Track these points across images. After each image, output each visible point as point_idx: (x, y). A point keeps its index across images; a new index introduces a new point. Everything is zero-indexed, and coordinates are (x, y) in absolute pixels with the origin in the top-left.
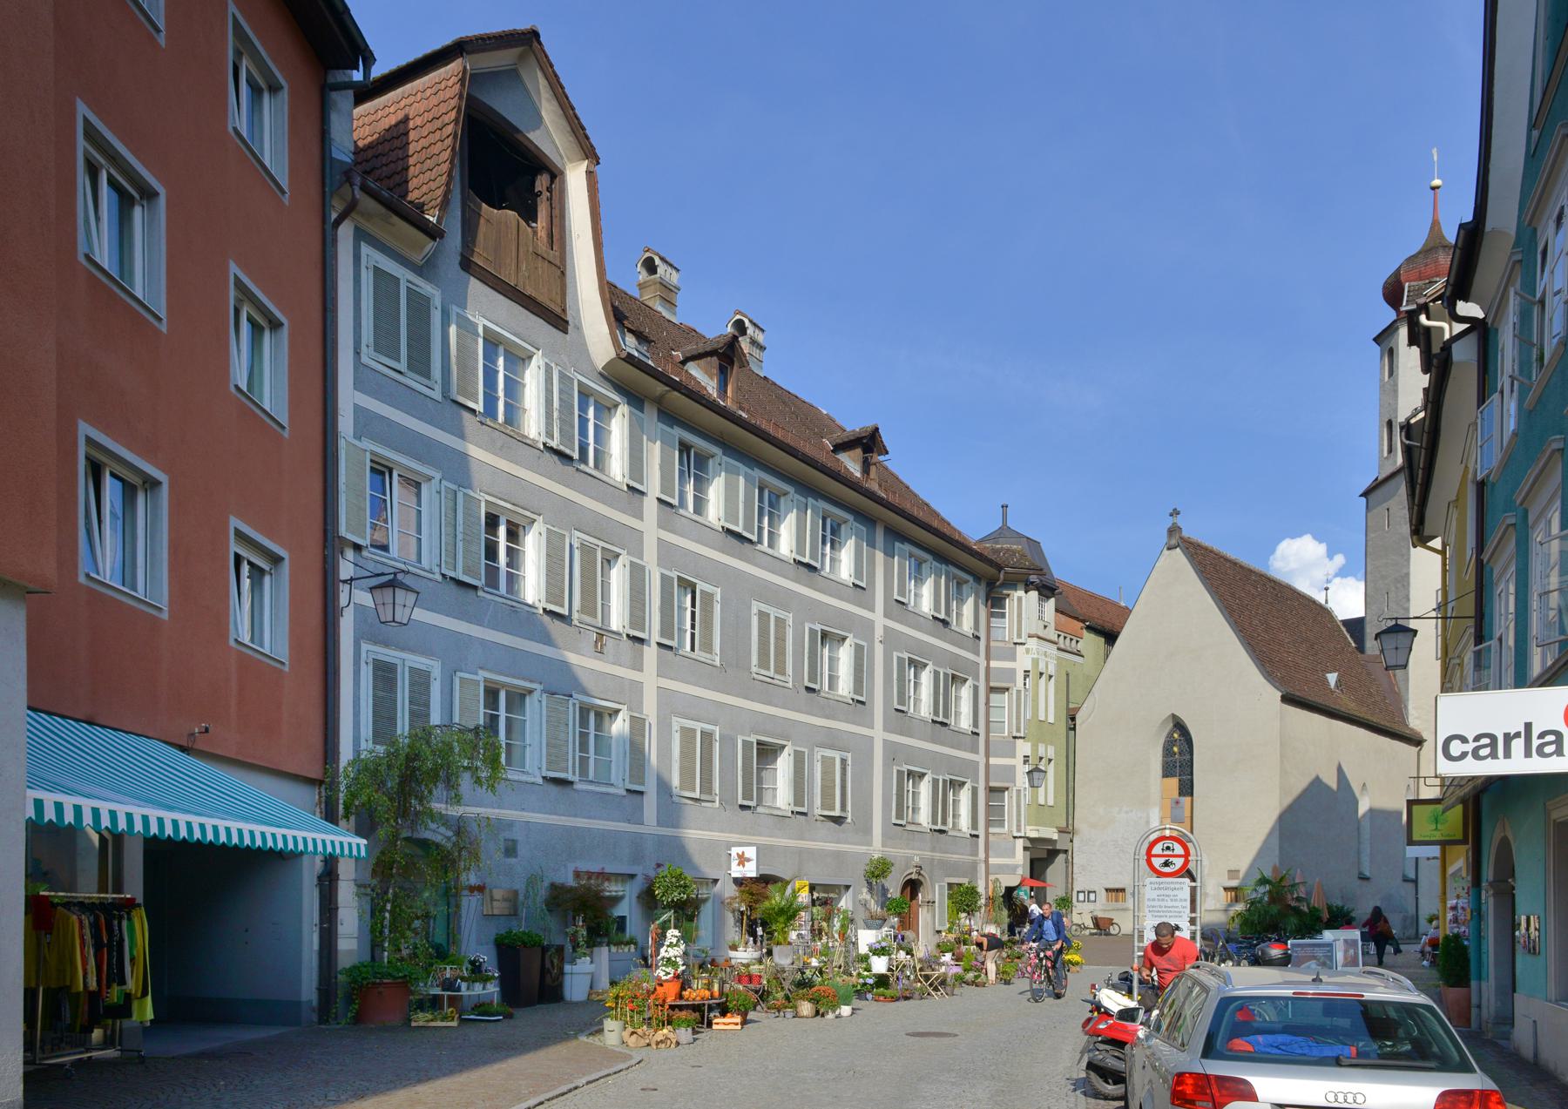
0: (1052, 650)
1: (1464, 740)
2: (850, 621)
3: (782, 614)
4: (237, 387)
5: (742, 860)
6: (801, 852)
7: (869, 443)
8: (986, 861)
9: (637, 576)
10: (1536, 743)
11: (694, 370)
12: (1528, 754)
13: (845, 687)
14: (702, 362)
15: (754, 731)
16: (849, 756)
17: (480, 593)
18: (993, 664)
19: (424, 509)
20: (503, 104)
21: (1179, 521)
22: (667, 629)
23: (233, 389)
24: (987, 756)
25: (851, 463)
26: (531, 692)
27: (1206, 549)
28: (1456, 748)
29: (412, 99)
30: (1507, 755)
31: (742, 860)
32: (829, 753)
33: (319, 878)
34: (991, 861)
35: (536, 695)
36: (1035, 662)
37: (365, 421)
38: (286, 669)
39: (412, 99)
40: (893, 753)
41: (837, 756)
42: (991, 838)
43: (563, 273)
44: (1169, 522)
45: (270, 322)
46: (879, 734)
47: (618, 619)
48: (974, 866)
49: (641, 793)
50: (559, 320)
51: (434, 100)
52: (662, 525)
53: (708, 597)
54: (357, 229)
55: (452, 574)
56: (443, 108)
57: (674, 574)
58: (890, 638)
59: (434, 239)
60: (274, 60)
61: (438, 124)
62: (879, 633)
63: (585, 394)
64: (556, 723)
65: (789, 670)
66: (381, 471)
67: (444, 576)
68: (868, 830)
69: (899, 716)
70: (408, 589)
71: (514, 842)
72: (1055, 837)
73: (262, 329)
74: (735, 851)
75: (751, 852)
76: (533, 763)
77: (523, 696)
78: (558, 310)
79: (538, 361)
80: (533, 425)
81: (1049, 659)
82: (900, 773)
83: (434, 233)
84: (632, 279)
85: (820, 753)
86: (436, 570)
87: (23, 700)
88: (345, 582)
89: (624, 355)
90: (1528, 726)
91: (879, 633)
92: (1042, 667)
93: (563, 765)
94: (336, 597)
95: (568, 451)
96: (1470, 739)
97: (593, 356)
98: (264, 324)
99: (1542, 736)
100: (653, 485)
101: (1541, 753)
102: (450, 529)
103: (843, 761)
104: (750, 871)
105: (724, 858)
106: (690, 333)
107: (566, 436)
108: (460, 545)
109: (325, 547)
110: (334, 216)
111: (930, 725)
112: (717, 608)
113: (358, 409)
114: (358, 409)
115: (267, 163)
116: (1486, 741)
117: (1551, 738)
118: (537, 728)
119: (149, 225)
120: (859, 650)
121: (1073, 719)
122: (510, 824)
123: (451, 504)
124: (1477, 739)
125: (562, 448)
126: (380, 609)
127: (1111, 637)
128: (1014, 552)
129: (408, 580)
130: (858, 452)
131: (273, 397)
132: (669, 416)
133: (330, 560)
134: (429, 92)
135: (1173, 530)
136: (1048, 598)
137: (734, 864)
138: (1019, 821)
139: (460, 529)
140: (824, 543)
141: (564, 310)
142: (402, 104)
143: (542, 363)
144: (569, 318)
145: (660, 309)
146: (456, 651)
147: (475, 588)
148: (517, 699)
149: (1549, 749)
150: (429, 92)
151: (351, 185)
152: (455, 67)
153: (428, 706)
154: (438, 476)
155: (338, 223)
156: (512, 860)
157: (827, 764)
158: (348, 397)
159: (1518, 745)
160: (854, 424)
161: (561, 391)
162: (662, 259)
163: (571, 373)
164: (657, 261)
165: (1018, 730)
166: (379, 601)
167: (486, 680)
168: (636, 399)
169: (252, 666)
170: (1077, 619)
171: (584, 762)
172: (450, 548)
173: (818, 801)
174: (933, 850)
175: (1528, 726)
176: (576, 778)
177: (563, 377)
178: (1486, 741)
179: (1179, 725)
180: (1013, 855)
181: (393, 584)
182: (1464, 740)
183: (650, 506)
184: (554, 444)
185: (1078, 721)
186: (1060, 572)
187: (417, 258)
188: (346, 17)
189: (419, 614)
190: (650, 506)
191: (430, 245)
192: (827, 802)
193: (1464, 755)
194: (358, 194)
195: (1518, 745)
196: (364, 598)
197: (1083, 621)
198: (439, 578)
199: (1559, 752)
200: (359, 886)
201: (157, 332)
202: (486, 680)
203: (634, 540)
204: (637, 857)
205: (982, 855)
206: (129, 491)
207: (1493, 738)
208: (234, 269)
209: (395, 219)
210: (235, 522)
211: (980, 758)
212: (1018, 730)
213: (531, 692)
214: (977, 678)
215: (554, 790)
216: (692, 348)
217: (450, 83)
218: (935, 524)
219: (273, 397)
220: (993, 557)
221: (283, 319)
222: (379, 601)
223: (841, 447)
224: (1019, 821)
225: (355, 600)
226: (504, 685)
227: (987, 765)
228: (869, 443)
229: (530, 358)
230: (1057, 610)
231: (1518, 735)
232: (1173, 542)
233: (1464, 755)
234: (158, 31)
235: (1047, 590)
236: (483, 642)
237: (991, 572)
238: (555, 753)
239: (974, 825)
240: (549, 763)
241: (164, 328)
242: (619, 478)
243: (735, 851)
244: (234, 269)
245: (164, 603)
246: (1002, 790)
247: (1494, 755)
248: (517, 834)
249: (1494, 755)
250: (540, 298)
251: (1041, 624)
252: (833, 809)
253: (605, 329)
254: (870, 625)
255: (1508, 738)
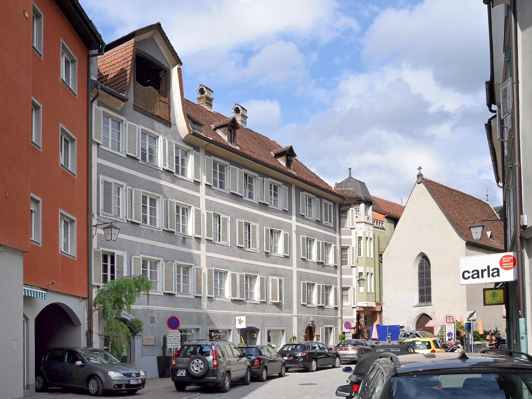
0: (371, 228)
1: (469, 272)
2: (281, 225)
3: (254, 224)
4: (61, 165)
5: (240, 322)
6: (264, 317)
7: (289, 154)
8: (341, 318)
9: (198, 213)
10: (491, 272)
11: (219, 132)
12: (489, 276)
13: (280, 251)
14: (222, 129)
15: (244, 270)
16: (283, 278)
17: (140, 226)
18: (342, 237)
19: (120, 197)
20: (150, 52)
21: (422, 172)
22: (209, 234)
23: (60, 165)
24: (341, 274)
25: (282, 161)
26: (159, 261)
27: (434, 182)
28: (466, 275)
29: (117, 52)
30: (482, 277)
31: (240, 322)
32: (274, 278)
33: (87, 333)
34: (344, 317)
35: (161, 262)
36: (365, 233)
37: (102, 169)
38: (76, 259)
39: (117, 52)
40: (301, 276)
41: (278, 279)
42: (343, 308)
43: (169, 107)
44: (417, 172)
45: (35, 107)
46: (294, 268)
47: (191, 231)
48: (336, 319)
49: (201, 297)
50: (168, 122)
51: (124, 53)
52: (207, 194)
53: (225, 220)
54: (98, 102)
55: (130, 220)
56: (128, 55)
57: (212, 212)
58: (299, 231)
59: (124, 101)
60: (73, 53)
61: (126, 61)
62: (294, 228)
63: (177, 148)
64: (168, 272)
65: (332, 221)
66: (107, 185)
67: (128, 221)
68: (291, 307)
69: (304, 261)
70: (116, 228)
71: (153, 318)
72: (375, 306)
73: (68, 142)
74: (237, 318)
75: (243, 318)
76: (160, 288)
77: (156, 263)
78: (167, 119)
79: (161, 138)
80: (160, 162)
81: (370, 231)
82: (304, 284)
83: (124, 100)
84: (193, 97)
85: (271, 278)
86: (125, 219)
87: (23, 283)
88: (94, 226)
89: (192, 133)
90: (488, 267)
91: (294, 228)
92: (367, 235)
93: (171, 288)
94: (91, 232)
95: (172, 170)
96: (471, 272)
97: (180, 134)
98: (69, 140)
99: (493, 270)
100: (204, 180)
101: (493, 276)
102: (130, 204)
103: (280, 280)
104: (243, 326)
105: (233, 321)
106: (218, 116)
107: (171, 165)
108: (133, 209)
109: (88, 214)
110: (91, 99)
111: (316, 264)
112: (229, 224)
113: (98, 164)
114: (98, 164)
115: (71, 87)
116: (476, 272)
117: (496, 271)
118: (161, 275)
119: (73, 148)
120: (286, 235)
121: (381, 255)
122: (152, 311)
123: (130, 194)
124: (473, 272)
125: (169, 169)
126: (107, 236)
127: (394, 220)
128: (350, 191)
129: (116, 225)
130: (284, 158)
131: (72, 167)
132: (209, 153)
133: (89, 219)
134: (123, 50)
135: (420, 176)
136: (369, 206)
137: (237, 323)
138: (354, 301)
139: (133, 203)
140: (271, 194)
141: (170, 119)
142: (113, 54)
143: (162, 139)
144: (172, 121)
145: (206, 107)
146: (131, 248)
147: (139, 224)
148: (155, 264)
149: (495, 274)
150: (123, 50)
151: (97, 88)
152: (132, 41)
153: (122, 269)
154: (125, 184)
155: (92, 101)
156: (153, 324)
157: (274, 281)
158: (95, 160)
159: (486, 273)
160: (284, 145)
161: (169, 148)
162: (206, 88)
163: (173, 141)
164: (205, 89)
165: (353, 264)
166: (106, 233)
167: (143, 258)
168: (197, 148)
169: (66, 259)
170: (382, 214)
171: (179, 286)
172: (130, 210)
173: (271, 297)
174: (318, 314)
175: (488, 267)
176: (176, 293)
177: (170, 143)
178: (476, 272)
179: (424, 257)
180: (352, 315)
181: (111, 227)
182: (469, 272)
183: (203, 188)
184: (166, 168)
185: (383, 256)
186: (374, 193)
187: (119, 109)
188: (90, 24)
189: (121, 236)
190: (203, 188)
191: (123, 104)
192: (274, 298)
193: (469, 277)
194: (100, 91)
195: (486, 273)
196: (101, 231)
197: (384, 214)
198: (126, 222)
199: (498, 275)
200: (100, 335)
201: (40, 152)
202: (143, 258)
203: (196, 201)
204: (199, 322)
205: (339, 315)
206: (66, 223)
207: (478, 271)
208: (61, 125)
209: (111, 97)
210: (61, 211)
211: (338, 276)
212: (353, 264)
213: (159, 261)
214: (335, 243)
215: (167, 297)
216: (218, 123)
217: (130, 47)
218: (316, 183)
219: (72, 167)
220: (341, 194)
221: (75, 138)
222: (106, 233)
223: (278, 155)
224: (354, 301)
225: (98, 232)
226: (149, 259)
227: (341, 279)
228: (289, 154)
229: (158, 137)
230: (373, 210)
231: (485, 270)
232: (420, 180)
233: (469, 277)
234: (41, 56)
235: (369, 202)
236: (142, 244)
237: (341, 201)
238: (168, 285)
239: (336, 303)
240: (166, 287)
241: (41, 151)
242: (190, 178)
243: (237, 318)
244: (61, 125)
245: (40, 242)
246: (347, 289)
247: (478, 277)
248: (155, 315)
249: (478, 277)
250: (161, 116)
251: (366, 217)
252: (276, 299)
253: (185, 124)
254: (290, 225)
255: (483, 271)
